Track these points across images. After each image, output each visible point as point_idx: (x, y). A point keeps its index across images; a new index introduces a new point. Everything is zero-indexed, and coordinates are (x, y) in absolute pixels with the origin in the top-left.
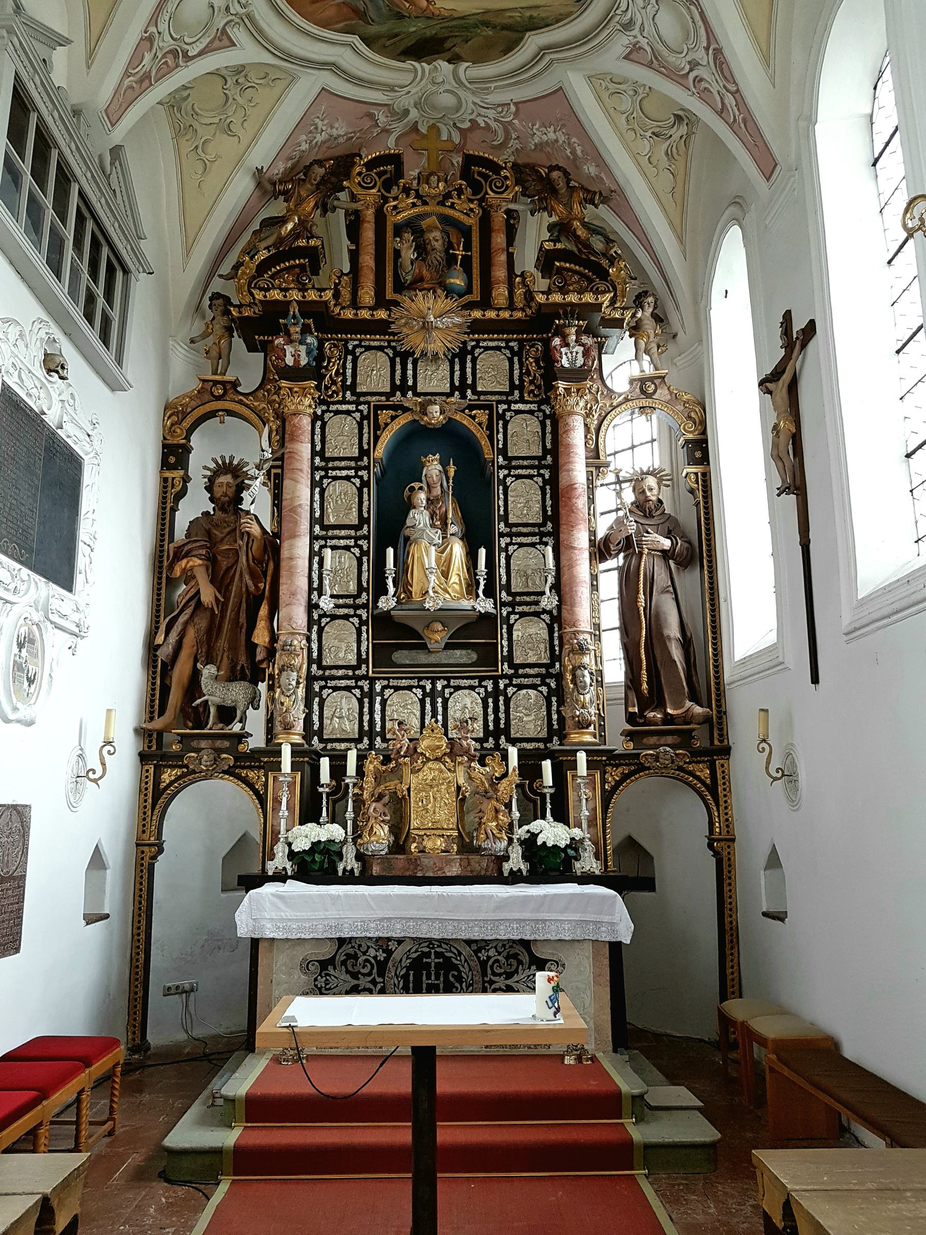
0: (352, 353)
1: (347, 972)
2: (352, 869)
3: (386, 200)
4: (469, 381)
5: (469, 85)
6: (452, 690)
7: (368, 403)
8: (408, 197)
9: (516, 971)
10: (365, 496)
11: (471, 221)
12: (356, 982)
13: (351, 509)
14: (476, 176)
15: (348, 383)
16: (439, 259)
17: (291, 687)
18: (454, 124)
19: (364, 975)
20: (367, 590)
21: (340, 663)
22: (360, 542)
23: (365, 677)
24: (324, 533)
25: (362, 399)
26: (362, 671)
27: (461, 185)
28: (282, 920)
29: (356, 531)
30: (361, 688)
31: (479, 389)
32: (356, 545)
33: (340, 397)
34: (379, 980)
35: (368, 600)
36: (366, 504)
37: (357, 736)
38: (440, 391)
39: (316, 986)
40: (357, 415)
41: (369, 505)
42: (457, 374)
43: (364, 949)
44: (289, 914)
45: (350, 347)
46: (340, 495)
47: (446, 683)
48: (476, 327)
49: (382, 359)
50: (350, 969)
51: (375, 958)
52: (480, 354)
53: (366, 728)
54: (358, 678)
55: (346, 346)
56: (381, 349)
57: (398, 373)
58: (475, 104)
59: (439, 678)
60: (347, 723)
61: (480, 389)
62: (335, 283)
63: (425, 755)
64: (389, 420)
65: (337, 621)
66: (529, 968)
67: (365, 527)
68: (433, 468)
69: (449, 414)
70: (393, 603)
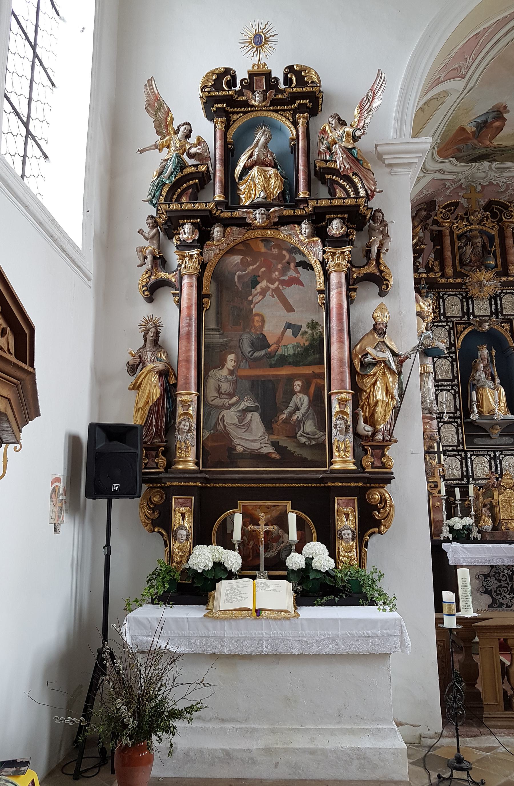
0: (442, 297)
1: (496, 579)
2: (477, 538)
3: (453, 224)
4: (500, 310)
5: (495, 170)
6: (504, 456)
7: (453, 322)
8: (463, 221)
9: (497, 588)
10: (455, 366)
11: (494, 232)
12: (500, 584)
13: (449, 372)
14: (495, 210)
15: (442, 312)
16: (480, 251)
17: (185, 431)
18: (480, 183)
19: (503, 581)
20: (460, 410)
21: (450, 444)
22: (454, 388)
23: (463, 450)
24: (437, 383)
25: (449, 320)
26: (461, 447)
27: (488, 214)
28: (467, 558)
29: (452, 382)
30: (461, 455)
31: (504, 313)
32: (452, 389)
33: (438, 320)
34: (510, 583)
35: (461, 414)
36: (455, 370)
37: (461, 478)
38: (485, 315)
39: (483, 585)
40: (447, 327)
41: (457, 370)
42: (493, 306)
43: (502, 570)
44: (470, 555)
45: (441, 295)
46: (443, 365)
47: (500, 453)
48: (503, 285)
49: (457, 300)
50: (497, 578)
51: (507, 573)
52: (503, 296)
53: (465, 474)
54: (459, 451)
55: (439, 294)
56: (456, 295)
57: (465, 307)
58: (495, 176)
59: (497, 451)
60: (455, 472)
61: (505, 313)
62: (432, 265)
63: (504, 487)
64: (462, 330)
65: (446, 425)
66: (491, 589)
67: (456, 380)
68: (484, 352)
69: (491, 326)
70: (477, 417)
